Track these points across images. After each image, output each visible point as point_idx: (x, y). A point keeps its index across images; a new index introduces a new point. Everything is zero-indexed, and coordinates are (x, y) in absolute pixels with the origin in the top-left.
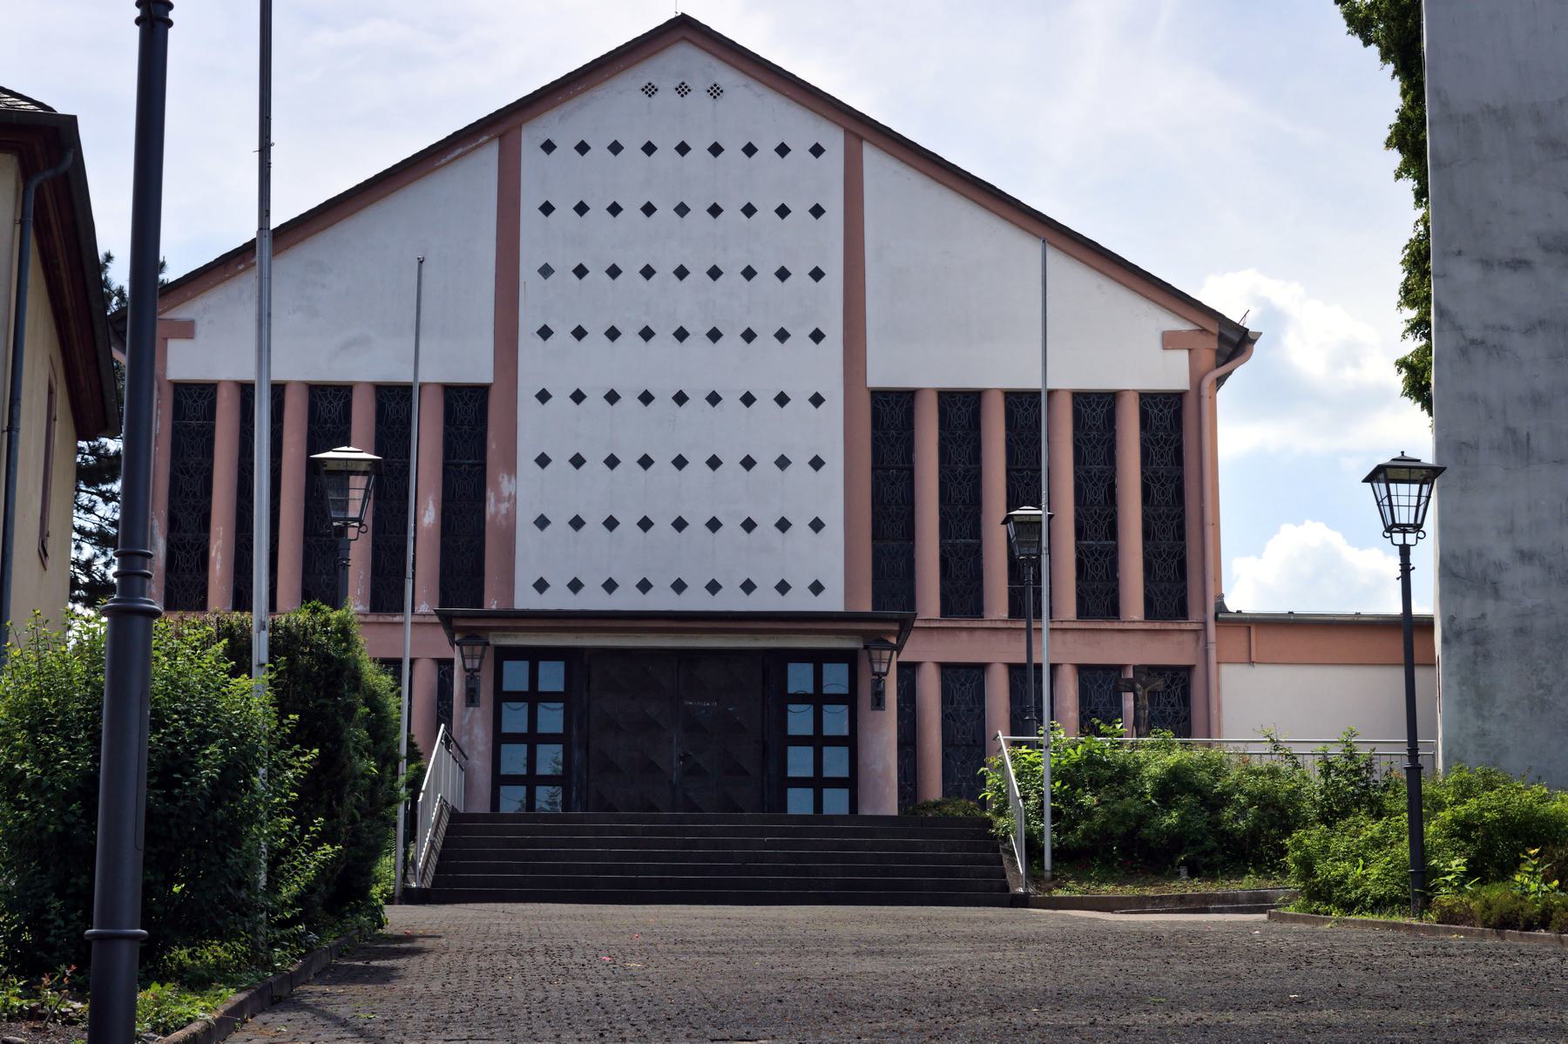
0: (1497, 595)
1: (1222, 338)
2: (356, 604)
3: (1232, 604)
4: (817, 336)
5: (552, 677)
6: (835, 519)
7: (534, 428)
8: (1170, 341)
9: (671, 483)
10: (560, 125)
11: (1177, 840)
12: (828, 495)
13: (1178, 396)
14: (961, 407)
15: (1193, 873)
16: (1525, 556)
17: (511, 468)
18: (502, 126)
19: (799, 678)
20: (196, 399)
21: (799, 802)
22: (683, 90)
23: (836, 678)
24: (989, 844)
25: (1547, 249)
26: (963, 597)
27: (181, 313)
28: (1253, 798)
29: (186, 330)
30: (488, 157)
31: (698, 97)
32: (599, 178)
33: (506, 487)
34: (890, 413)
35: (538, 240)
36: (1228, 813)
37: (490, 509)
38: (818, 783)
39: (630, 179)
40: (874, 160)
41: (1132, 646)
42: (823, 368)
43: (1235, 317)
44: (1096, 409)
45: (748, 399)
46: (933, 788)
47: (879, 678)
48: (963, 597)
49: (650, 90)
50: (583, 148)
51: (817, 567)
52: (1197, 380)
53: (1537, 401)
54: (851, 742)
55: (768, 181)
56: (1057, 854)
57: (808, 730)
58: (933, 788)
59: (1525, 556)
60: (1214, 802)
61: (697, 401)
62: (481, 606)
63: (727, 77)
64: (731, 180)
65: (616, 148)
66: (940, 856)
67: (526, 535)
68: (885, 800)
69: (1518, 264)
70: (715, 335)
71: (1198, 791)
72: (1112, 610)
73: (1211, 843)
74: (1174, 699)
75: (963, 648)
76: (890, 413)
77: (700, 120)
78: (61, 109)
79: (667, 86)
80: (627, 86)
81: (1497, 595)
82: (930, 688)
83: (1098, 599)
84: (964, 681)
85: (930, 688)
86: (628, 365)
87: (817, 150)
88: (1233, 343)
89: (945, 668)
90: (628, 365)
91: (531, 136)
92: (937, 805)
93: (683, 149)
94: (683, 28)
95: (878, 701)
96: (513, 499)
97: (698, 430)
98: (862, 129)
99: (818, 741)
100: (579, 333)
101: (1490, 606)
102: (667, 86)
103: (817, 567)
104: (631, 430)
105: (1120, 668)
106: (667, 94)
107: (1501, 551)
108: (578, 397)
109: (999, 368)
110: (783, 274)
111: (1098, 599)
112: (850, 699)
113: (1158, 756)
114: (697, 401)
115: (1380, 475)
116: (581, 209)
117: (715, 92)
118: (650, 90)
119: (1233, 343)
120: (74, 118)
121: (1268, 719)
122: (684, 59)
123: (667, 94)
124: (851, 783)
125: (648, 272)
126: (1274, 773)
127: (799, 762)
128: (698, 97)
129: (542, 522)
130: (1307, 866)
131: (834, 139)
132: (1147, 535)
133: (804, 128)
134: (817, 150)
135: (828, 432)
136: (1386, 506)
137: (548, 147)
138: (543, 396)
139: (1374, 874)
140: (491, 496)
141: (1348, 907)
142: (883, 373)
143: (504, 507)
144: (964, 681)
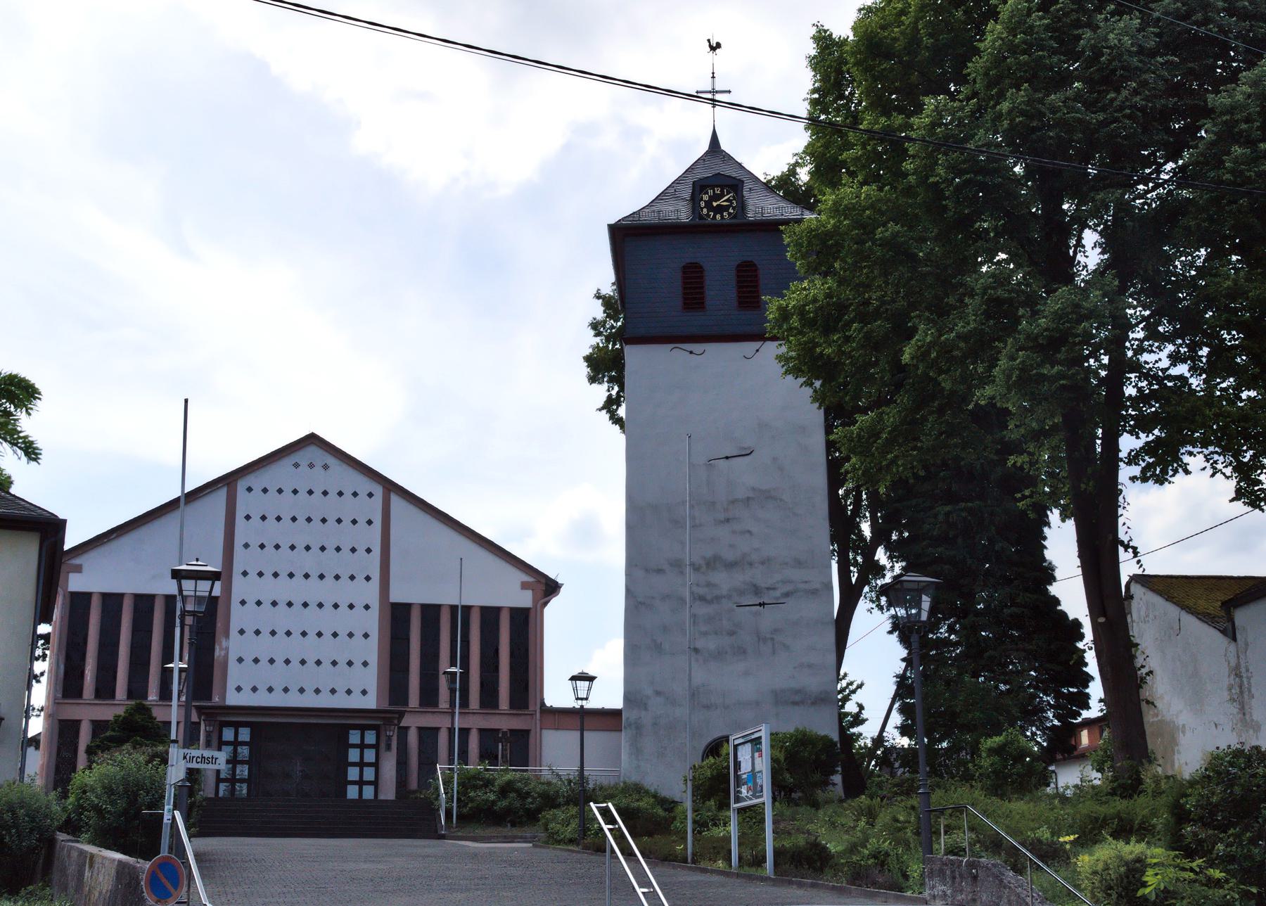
0: (646, 709)
1: (547, 584)
2: (153, 696)
3: (548, 703)
4: (368, 578)
5: (245, 734)
6: (373, 659)
7: (239, 617)
8: (525, 586)
9: (302, 648)
10: (254, 480)
11: (508, 811)
12: (371, 650)
13: (527, 610)
14: (431, 612)
15: (513, 825)
16: (658, 693)
17: (227, 635)
18: (229, 481)
19: (354, 737)
20: (80, 601)
21: (352, 792)
22: (311, 466)
23: (370, 738)
24: (430, 809)
25: (671, 565)
26: (429, 697)
27: (77, 561)
28: (540, 795)
29: (78, 569)
30: (221, 495)
31: (318, 469)
32: (272, 504)
33: (224, 644)
34: (397, 615)
35: (243, 531)
36: (530, 800)
37: (217, 653)
38: (361, 783)
39: (286, 506)
40: (395, 500)
41: (503, 723)
42: (370, 594)
43: (552, 576)
44: (490, 615)
45: (335, 635)
46: (413, 785)
47: (389, 738)
48: (429, 697)
49: (296, 465)
50: (265, 491)
51: (361, 688)
52: (535, 601)
53: (665, 629)
54: (376, 765)
55: (349, 508)
56: (460, 817)
57: (357, 760)
58: (413, 785)
59: (658, 693)
60: (523, 796)
61: (313, 606)
62: (210, 698)
63: (331, 461)
64: (332, 507)
65: (280, 491)
66: (408, 817)
67: (233, 666)
68: (389, 792)
69: (660, 571)
70: (322, 577)
71: (518, 791)
72: (495, 705)
73: (521, 813)
74: (519, 746)
75: (429, 721)
76: (397, 615)
77: (319, 480)
78: (61, 517)
79: (304, 464)
80: (287, 462)
81: (646, 709)
82: (413, 738)
83: (489, 698)
84: (428, 735)
85: (413, 738)
86: (284, 589)
87: (370, 495)
88: (550, 588)
89: (420, 729)
90: (284, 589)
91: (241, 485)
92: (414, 792)
93: (310, 492)
94: (312, 440)
95: (389, 748)
96: (227, 649)
97: (313, 619)
98: (390, 487)
99: (361, 764)
100: (260, 574)
101: (643, 713)
102: (304, 464)
103: (361, 688)
104: (283, 619)
105: (497, 730)
106: (304, 467)
107: (649, 691)
108: (259, 603)
109: (446, 596)
110: (353, 550)
111: (489, 698)
112: (376, 747)
113: (504, 773)
114: (313, 606)
115: (574, 678)
116: (264, 518)
117: (326, 467)
118: (296, 465)
119: (550, 588)
120: (65, 521)
121: (557, 756)
122: (313, 452)
123: (304, 467)
124: (375, 784)
125: (293, 547)
126: (549, 784)
127: (353, 774)
128: (318, 469)
129: (240, 660)
130: (546, 825)
131: (378, 491)
132: (512, 669)
133: (365, 485)
134: (370, 495)
135: (372, 622)
136: (575, 689)
137: (250, 489)
138: (243, 603)
139: (570, 830)
140: (217, 647)
141: (559, 842)
142: (396, 596)
143: (223, 653)
144: (428, 735)
